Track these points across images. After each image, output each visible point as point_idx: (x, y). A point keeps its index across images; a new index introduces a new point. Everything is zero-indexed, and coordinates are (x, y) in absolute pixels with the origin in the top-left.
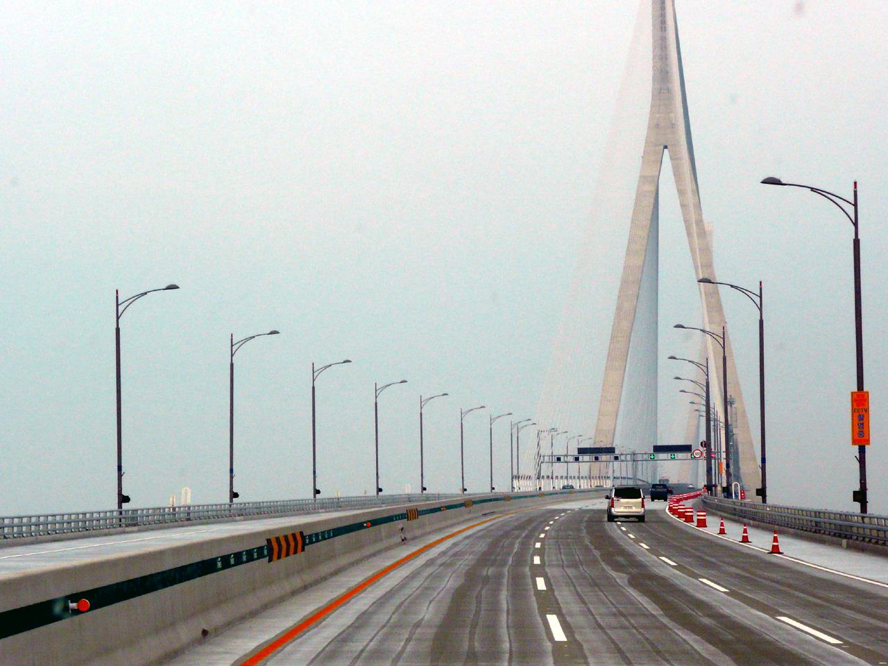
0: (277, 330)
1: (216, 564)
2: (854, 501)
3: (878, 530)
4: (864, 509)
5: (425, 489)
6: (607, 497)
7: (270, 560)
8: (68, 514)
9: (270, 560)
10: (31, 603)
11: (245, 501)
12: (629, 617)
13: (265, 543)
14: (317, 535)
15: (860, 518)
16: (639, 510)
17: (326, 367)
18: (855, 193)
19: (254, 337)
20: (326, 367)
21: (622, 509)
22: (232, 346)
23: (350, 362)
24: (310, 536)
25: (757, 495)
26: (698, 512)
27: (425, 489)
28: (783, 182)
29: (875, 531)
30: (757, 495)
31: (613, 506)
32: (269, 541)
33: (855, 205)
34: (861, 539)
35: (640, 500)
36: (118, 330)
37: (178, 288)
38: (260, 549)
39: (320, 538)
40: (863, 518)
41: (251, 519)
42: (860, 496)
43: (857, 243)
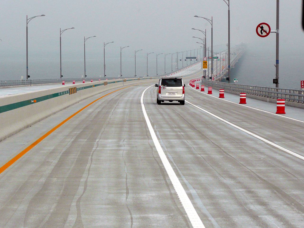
0: (44, 15)
1: (61, 94)
2: (273, 83)
3: (256, 91)
4: (277, 86)
5: (29, 77)
6: (157, 86)
7: (70, 94)
8: (1, 81)
9: (70, 94)
10: (279, 52)
11: (88, 78)
12: (173, 207)
13: (68, 90)
14: (81, 88)
15: (276, 90)
16: (180, 96)
17: (33, 18)
18: (212, 19)
19: (35, 17)
20: (33, 18)
21: (167, 95)
22: (27, 20)
23: (74, 28)
24: (78, 88)
25: (274, 83)
26: (208, 87)
27: (29, 77)
28: (198, 16)
29: (265, 92)
30: (274, 83)
31: (160, 92)
32: (69, 89)
33: (212, 21)
34: (252, 94)
35: (181, 88)
36: (27, 27)
37: (45, 16)
38: (67, 91)
39: (83, 88)
40: (277, 90)
41: (8, 88)
42: (276, 81)
43: (229, 11)
